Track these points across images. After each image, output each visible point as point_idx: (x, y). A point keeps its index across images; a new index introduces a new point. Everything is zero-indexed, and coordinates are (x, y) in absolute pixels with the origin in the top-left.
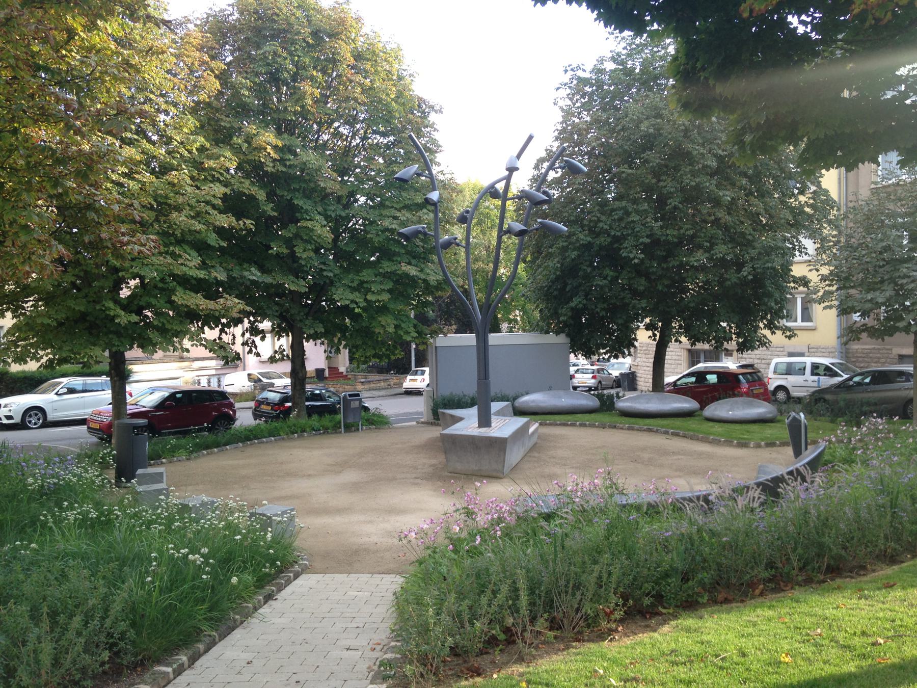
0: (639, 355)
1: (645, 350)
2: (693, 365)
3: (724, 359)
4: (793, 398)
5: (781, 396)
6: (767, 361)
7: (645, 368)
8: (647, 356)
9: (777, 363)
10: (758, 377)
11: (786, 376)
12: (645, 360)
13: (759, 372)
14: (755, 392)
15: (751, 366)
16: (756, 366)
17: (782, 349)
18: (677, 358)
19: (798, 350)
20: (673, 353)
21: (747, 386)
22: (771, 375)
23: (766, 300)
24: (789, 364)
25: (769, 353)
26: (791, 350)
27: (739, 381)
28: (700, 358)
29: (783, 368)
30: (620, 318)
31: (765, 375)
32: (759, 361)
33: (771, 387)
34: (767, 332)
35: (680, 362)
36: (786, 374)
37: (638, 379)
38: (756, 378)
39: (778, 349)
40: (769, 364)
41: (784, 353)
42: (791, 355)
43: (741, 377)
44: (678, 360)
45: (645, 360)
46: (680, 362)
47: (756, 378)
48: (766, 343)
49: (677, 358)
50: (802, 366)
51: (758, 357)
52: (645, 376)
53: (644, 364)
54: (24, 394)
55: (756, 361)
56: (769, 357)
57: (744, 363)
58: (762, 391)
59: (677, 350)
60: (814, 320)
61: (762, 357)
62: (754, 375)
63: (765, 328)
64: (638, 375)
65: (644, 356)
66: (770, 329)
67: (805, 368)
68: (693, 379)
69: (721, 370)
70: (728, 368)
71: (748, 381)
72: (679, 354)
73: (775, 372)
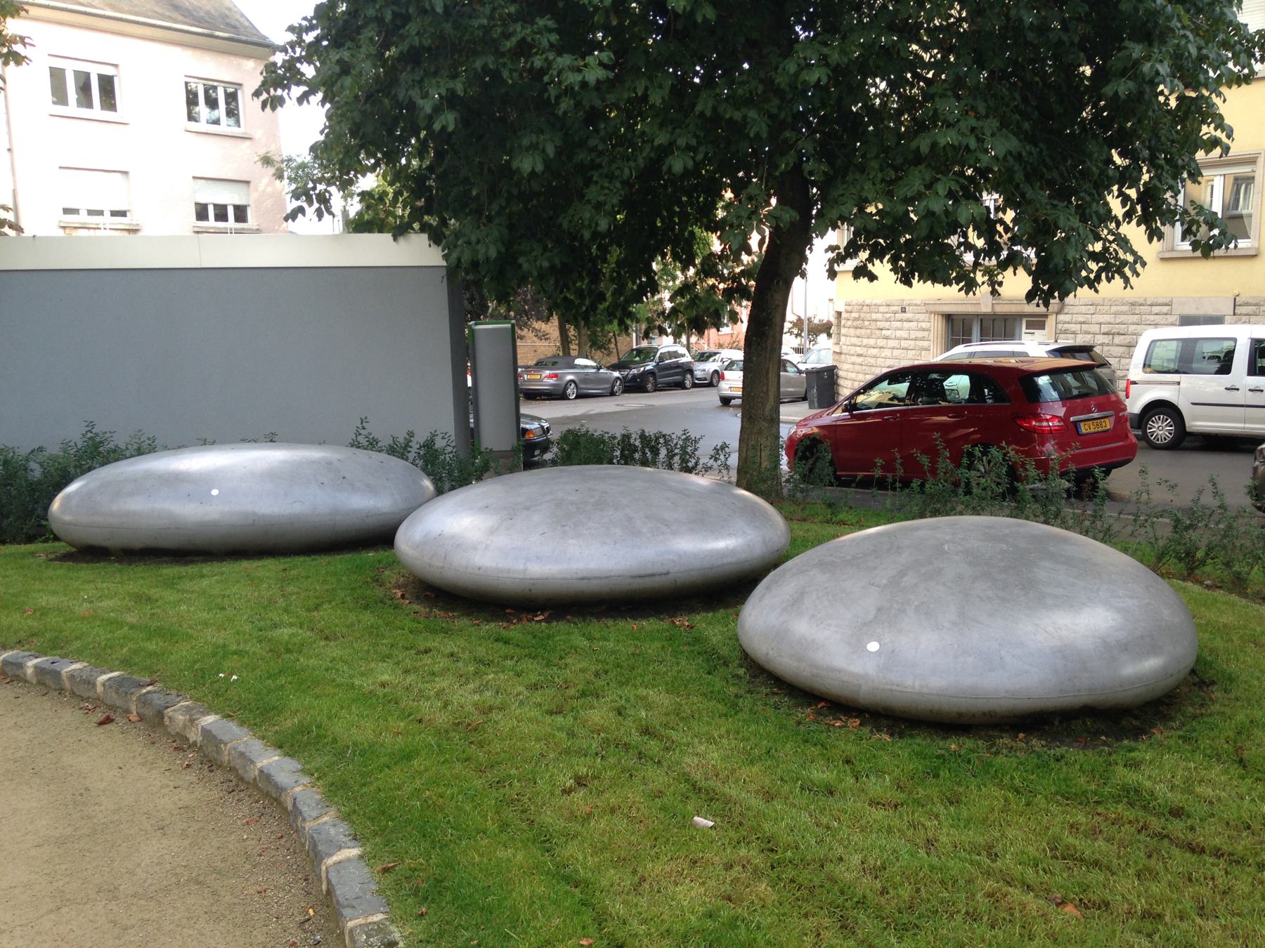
0: (843, 331)
1: (856, 319)
2: (948, 349)
3: (1024, 336)
4: (1192, 434)
5: (1161, 429)
6: (1127, 339)
7: (854, 359)
8: (858, 332)
9: (1154, 342)
10: (1099, 380)
11: (1175, 377)
12: (854, 340)
13: (1104, 364)
14: (1084, 429)
15: (1086, 350)
16: (1097, 350)
17: (1165, 309)
18: (920, 334)
19: (1209, 310)
20: (913, 325)
21: (1061, 412)
22: (1136, 373)
23: (1137, 50)
24: (1188, 344)
25: (1135, 318)
26: (1190, 310)
27: (1036, 390)
28: (970, 334)
29: (1168, 353)
30: (534, 147)
31: (1119, 373)
32: (1106, 339)
33: (1135, 405)
34: (1135, 233)
35: (925, 344)
36: (1177, 372)
37: (841, 382)
38: (1093, 384)
39: (1156, 309)
40: (1131, 346)
41: (1171, 319)
42: (1187, 321)
43: (1043, 381)
44: (923, 339)
45: (854, 340)
46: (925, 344)
47: (1093, 384)
48: (1125, 263)
49: (920, 334)
50: (1227, 345)
51: (1105, 328)
52: (853, 375)
53: (853, 350)
54: (453, 375)
55: (1100, 339)
56: (1132, 328)
57: (1065, 342)
58: (1108, 424)
59: (921, 317)
60: (1252, 233)
61: (1115, 329)
62: (1086, 375)
63: (1129, 215)
64: (841, 373)
65: (852, 331)
66: (1146, 220)
67: (1230, 355)
68: (902, 388)
69: (989, 362)
70: (1025, 354)
71: (1065, 397)
72: (924, 325)
73: (1146, 365)
